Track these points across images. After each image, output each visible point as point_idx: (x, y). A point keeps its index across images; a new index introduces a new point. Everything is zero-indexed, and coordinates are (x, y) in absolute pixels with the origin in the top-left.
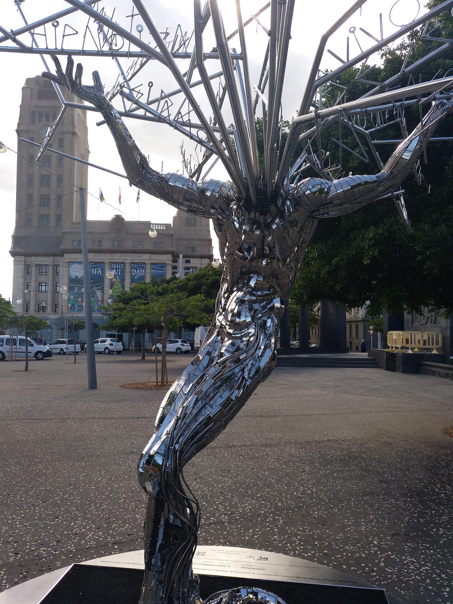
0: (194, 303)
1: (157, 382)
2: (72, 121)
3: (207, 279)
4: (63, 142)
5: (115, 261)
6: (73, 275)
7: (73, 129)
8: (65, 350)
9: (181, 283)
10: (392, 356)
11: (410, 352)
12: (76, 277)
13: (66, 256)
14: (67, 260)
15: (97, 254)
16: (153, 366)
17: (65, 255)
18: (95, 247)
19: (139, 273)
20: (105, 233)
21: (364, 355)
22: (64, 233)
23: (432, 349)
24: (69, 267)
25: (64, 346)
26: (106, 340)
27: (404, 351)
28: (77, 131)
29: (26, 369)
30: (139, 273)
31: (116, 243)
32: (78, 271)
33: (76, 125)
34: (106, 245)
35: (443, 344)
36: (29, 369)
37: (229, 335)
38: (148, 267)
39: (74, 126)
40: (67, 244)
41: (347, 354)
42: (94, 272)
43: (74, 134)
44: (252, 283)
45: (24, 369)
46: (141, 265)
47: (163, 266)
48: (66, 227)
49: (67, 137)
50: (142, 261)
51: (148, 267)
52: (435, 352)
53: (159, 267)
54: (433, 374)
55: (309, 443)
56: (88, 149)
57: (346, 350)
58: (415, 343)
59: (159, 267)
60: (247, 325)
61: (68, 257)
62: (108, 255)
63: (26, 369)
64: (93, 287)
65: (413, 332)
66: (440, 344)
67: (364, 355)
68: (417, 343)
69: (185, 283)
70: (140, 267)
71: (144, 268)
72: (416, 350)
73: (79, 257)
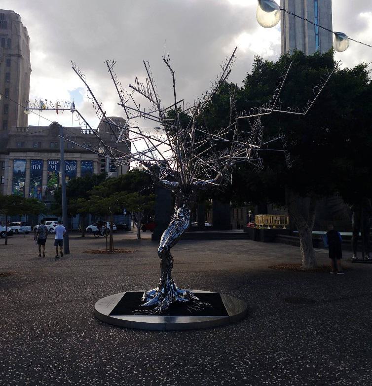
0: (132, 198)
1: (107, 250)
2: (18, 46)
3: (135, 179)
4: (10, 63)
5: (52, 159)
6: (17, 170)
7: (19, 52)
8: (19, 231)
9: (115, 182)
10: (258, 231)
11: (269, 228)
12: (19, 171)
13: (11, 154)
14: (12, 158)
15: (37, 153)
16: (104, 240)
17: (10, 153)
18: (36, 146)
19: (70, 168)
20: (44, 136)
21: (242, 231)
22: (10, 136)
23: (283, 227)
24: (13, 164)
25: (18, 227)
26: (51, 223)
27: (265, 228)
28: (22, 54)
29: (6, 244)
30: (70, 168)
31: (53, 145)
32: (20, 166)
33: (21, 49)
34: (45, 146)
35: (290, 223)
36: (8, 243)
37: (178, 220)
38: (79, 163)
39: (19, 50)
40: (12, 145)
41: (231, 230)
42: (35, 167)
43: (19, 56)
44: (184, 206)
45: (4, 244)
46: (74, 162)
47: (91, 163)
48: (12, 131)
49: (14, 59)
50: (74, 159)
51: (79, 163)
52: (284, 228)
53: (89, 163)
54: (283, 242)
55: (201, 271)
56: (30, 68)
57: (231, 228)
58: (283, 223)
59: (89, 163)
60: (182, 217)
61: (12, 155)
62: (46, 154)
63: (6, 244)
64: (33, 179)
65: (272, 215)
66: (288, 223)
67: (242, 231)
68: (274, 222)
69: (119, 182)
70: (72, 164)
71: (76, 165)
72: (274, 227)
73: (22, 155)
